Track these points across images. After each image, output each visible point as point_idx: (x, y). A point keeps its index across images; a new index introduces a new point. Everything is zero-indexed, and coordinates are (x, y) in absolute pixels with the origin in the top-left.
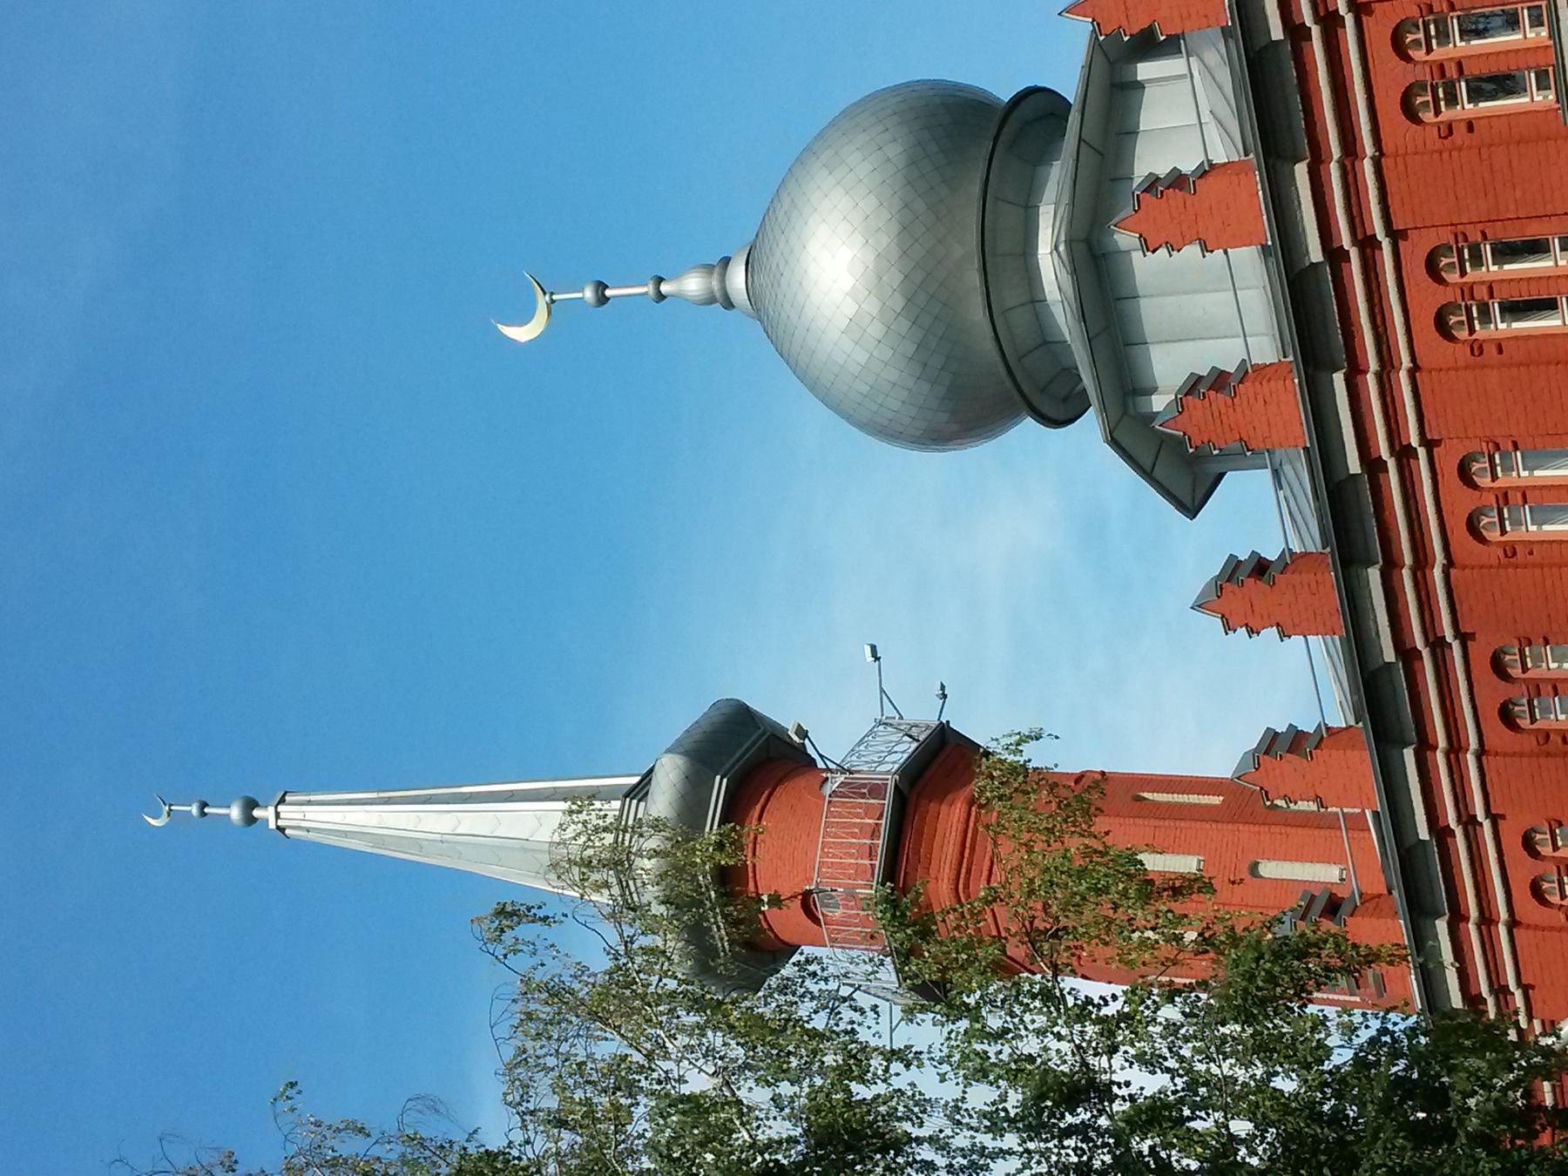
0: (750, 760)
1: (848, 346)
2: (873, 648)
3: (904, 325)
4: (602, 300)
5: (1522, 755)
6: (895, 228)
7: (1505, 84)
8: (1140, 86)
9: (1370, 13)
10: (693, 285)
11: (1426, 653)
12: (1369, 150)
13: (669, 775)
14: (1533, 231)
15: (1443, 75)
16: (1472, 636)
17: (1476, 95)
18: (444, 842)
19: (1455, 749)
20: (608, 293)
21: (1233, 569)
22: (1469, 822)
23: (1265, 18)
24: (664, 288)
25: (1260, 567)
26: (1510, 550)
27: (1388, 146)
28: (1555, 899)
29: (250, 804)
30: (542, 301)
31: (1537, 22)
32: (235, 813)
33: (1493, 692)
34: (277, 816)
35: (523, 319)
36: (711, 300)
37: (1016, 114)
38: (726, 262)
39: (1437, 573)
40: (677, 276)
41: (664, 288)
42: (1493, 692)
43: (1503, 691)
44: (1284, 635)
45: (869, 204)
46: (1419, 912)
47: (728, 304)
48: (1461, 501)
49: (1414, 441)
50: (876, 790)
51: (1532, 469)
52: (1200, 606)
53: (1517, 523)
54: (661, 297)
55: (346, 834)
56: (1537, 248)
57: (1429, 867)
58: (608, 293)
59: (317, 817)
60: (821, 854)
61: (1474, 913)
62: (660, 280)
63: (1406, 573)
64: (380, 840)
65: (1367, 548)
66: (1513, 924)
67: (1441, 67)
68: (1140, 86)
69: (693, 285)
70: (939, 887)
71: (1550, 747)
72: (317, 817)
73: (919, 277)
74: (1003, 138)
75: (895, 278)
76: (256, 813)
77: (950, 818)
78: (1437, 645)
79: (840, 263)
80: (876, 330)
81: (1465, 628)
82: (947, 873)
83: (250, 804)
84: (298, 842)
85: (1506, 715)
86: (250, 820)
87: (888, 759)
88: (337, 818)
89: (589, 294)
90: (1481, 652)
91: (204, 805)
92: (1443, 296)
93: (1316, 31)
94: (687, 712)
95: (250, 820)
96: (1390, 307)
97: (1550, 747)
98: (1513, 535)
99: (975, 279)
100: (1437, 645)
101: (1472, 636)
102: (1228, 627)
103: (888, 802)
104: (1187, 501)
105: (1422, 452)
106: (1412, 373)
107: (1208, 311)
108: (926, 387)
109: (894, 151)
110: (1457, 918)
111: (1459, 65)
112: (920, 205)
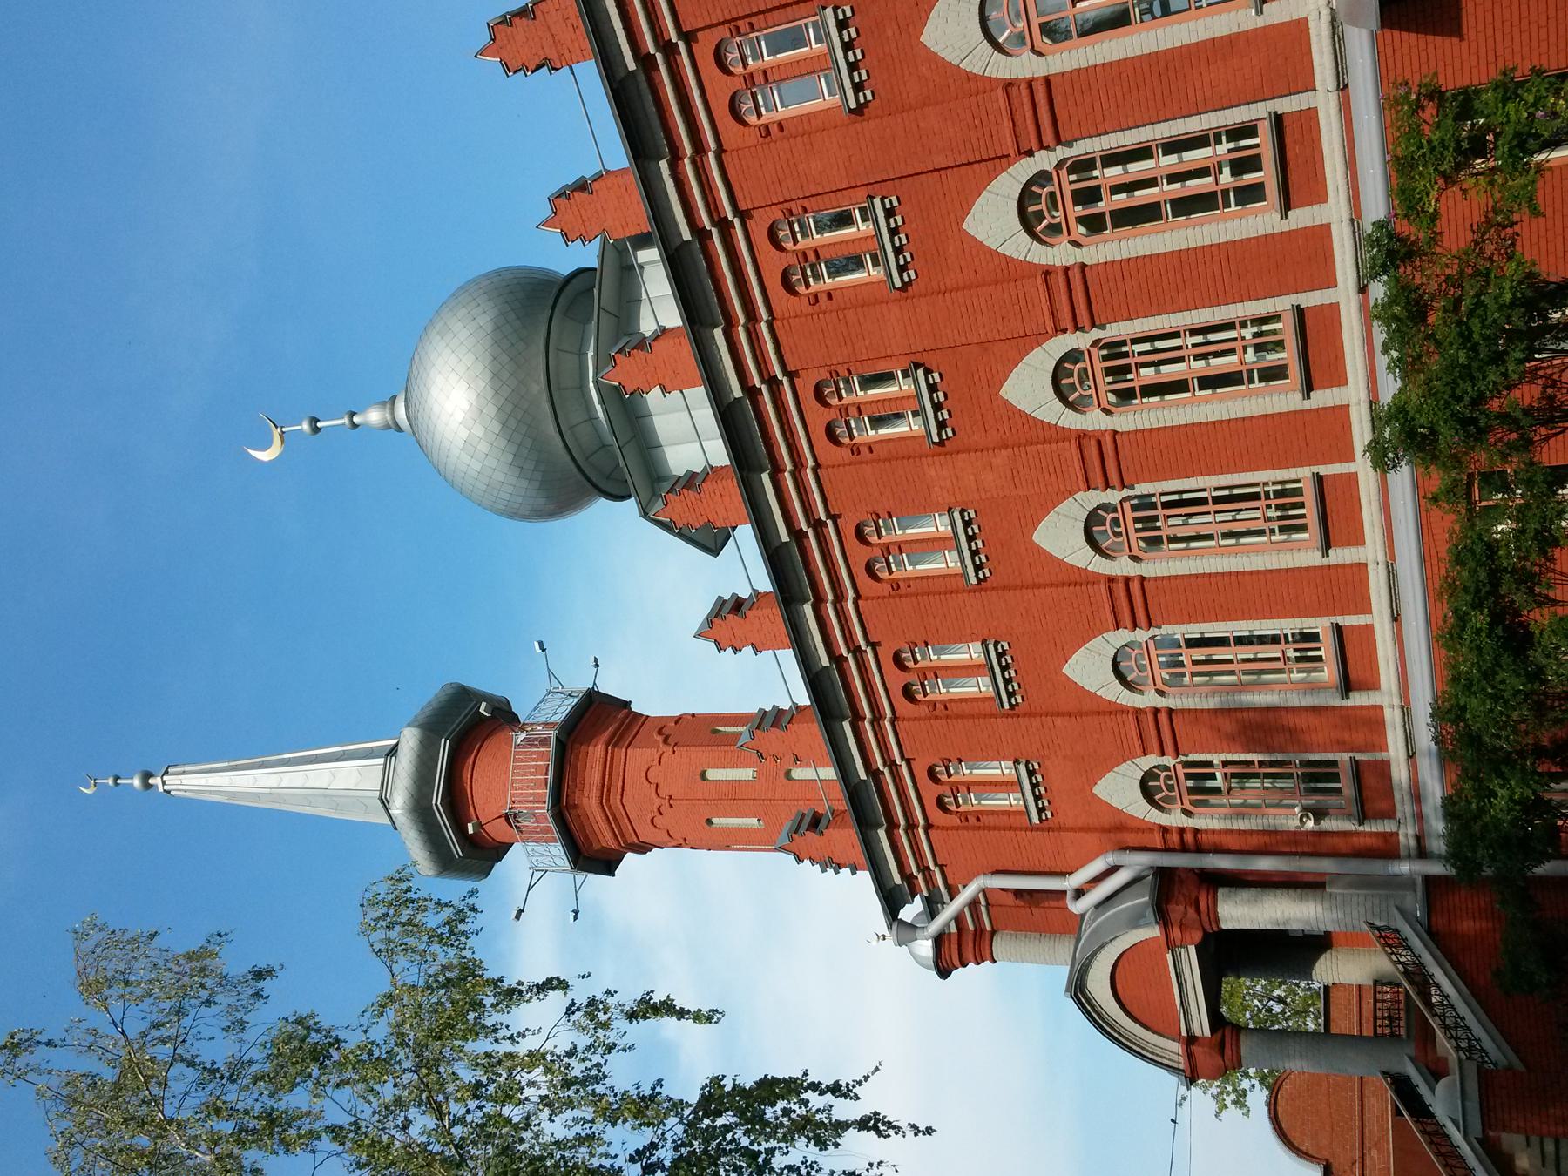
0: (466, 726)
1: (466, 459)
2: (541, 644)
3: (502, 443)
4: (316, 430)
5: (919, 719)
6: (488, 375)
7: (857, 263)
8: (641, 267)
9: (751, 217)
10: (374, 416)
11: (850, 657)
12: (765, 316)
13: (409, 740)
14: (882, 367)
15: (806, 260)
16: (879, 644)
17: (835, 271)
18: (272, 794)
19: (877, 718)
20: (319, 425)
21: (721, 604)
22: (892, 765)
23: (676, 225)
24: (356, 419)
25: (738, 605)
26: (895, 585)
27: (777, 311)
28: (953, 808)
29: (147, 775)
30: (276, 432)
31: (864, 220)
32: (137, 782)
33: (897, 679)
34: (164, 783)
35: (265, 446)
36: (387, 427)
37: (569, 287)
38: (394, 399)
39: (850, 604)
40: (364, 410)
41: (356, 419)
42: (897, 679)
43: (905, 678)
44: (757, 651)
45: (469, 359)
46: (865, 825)
47: (400, 430)
48: (860, 554)
49: (823, 517)
50: (545, 742)
51: (904, 528)
52: (699, 635)
53: (899, 564)
54: (355, 426)
55: (210, 792)
56: (886, 378)
57: (870, 798)
58: (319, 425)
59: (188, 782)
60: (513, 781)
61: (902, 822)
62: (353, 414)
63: (829, 605)
64: (233, 795)
65: (802, 591)
66: (928, 826)
67: (804, 254)
68: (641, 267)
69: (374, 416)
70: (589, 802)
71: (937, 712)
72: (188, 782)
73: (509, 408)
74: (559, 305)
75: (491, 410)
76: (151, 781)
77: (595, 753)
78: (857, 652)
79: (457, 399)
80: (483, 447)
81: (873, 639)
82: (595, 793)
83: (147, 775)
84: (179, 798)
85: (907, 692)
86: (147, 786)
87: (559, 710)
88: (203, 782)
89: (305, 426)
90: (886, 654)
91: (117, 778)
92: (830, 415)
93: (715, 232)
94: (426, 693)
95: (147, 786)
96: (796, 425)
97: (937, 712)
98: (897, 574)
99: (546, 407)
100: (857, 652)
101: (879, 644)
102: (720, 648)
103: (551, 750)
104: (711, 545)
105: (829, 522)
106: (815, 470)
107: (687, 434)
108: (525, 483)
109: (485, 320)
110: (892, 826)
111: (816, 252)
112: (505, 358)
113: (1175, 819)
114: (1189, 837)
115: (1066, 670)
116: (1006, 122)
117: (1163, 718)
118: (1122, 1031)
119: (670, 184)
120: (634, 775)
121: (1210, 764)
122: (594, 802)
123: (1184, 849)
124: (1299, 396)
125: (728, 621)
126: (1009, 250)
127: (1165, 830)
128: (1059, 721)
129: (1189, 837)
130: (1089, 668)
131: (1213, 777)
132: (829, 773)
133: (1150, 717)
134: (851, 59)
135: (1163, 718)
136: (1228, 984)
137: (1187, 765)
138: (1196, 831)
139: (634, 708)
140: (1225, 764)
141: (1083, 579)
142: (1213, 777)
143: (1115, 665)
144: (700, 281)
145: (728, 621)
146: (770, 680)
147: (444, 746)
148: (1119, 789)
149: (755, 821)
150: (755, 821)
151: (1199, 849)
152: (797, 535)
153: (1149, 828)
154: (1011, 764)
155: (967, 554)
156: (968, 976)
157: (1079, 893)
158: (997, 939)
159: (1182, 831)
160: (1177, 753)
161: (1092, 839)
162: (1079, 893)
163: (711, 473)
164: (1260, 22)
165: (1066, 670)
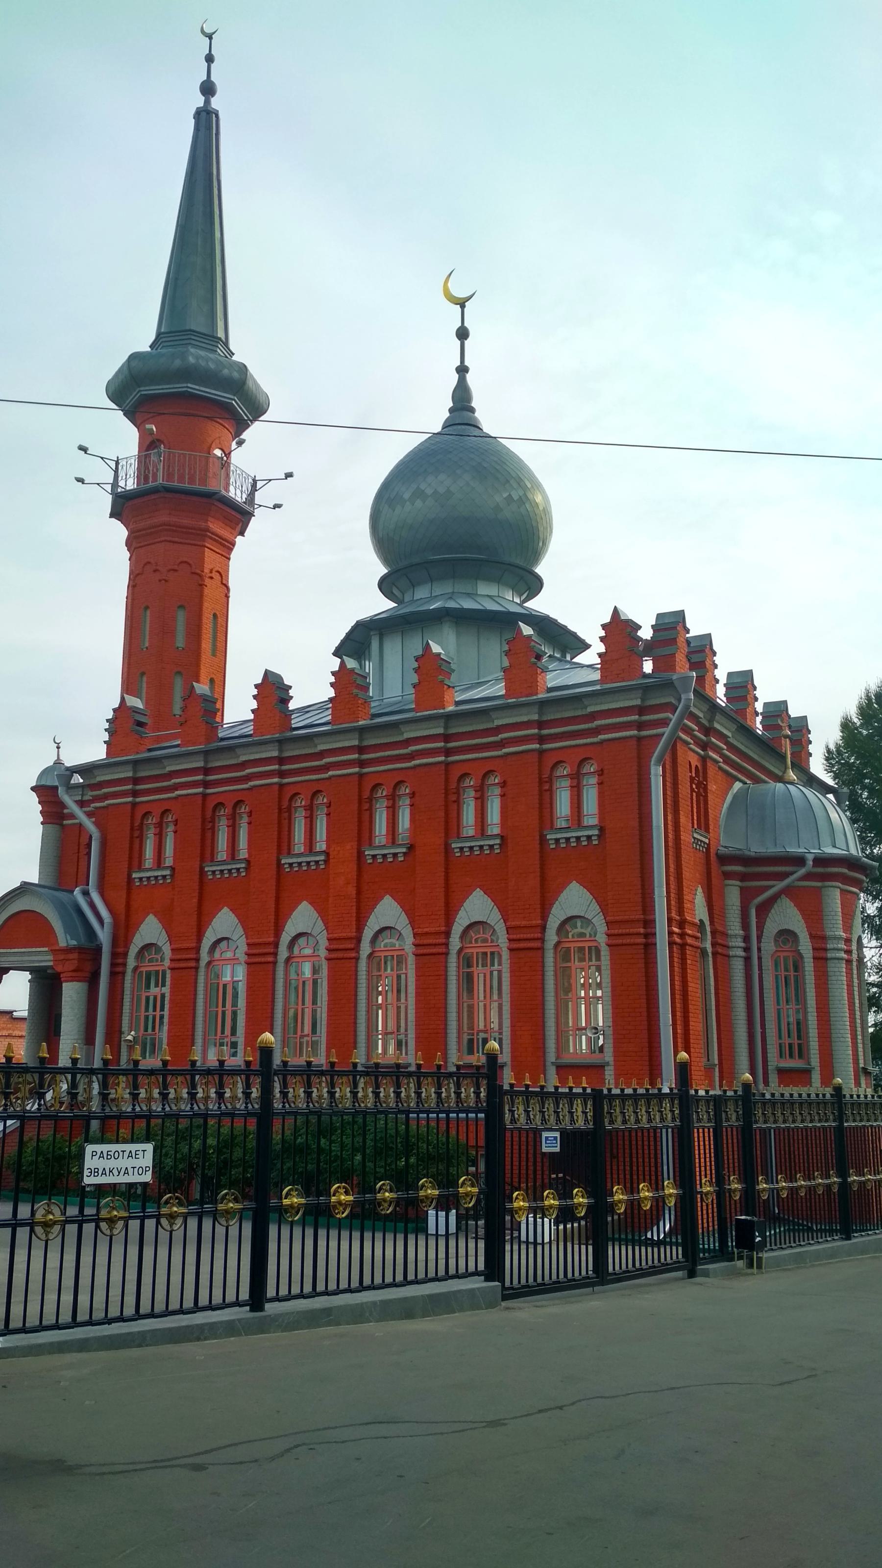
18: (60, 922)
113: (131, 962)
114: (119, 969)
115: (226, 910)
116: (524, 923)
117: (192, 964)
119: (525, 719)
121: (164, 985)
123: (113, 965)
125: (273, 691)
126: (461, 913)
127: (126, 954)
128: (195, 900)
129: (119, 969)
131: (157, 985)
133: (193, 956)
134: (572, 840)
135: (192, 964)
136: (27, 975)
137: (164, 972)
140: (163, 996)
142: (157, 985)
143: (227, 939)
145: (273, 691)
146: (238, 706)
148: (150, 930)
149: (147, 644)
150: (147, 644)
153: (127, 946)
154: (171, 864)
156: (33, 806)
157: (86, 893)
158: (57, 827)
161: (121, 908)
162: (86, 893)
164: (548, 1064)
165: (226, 910)
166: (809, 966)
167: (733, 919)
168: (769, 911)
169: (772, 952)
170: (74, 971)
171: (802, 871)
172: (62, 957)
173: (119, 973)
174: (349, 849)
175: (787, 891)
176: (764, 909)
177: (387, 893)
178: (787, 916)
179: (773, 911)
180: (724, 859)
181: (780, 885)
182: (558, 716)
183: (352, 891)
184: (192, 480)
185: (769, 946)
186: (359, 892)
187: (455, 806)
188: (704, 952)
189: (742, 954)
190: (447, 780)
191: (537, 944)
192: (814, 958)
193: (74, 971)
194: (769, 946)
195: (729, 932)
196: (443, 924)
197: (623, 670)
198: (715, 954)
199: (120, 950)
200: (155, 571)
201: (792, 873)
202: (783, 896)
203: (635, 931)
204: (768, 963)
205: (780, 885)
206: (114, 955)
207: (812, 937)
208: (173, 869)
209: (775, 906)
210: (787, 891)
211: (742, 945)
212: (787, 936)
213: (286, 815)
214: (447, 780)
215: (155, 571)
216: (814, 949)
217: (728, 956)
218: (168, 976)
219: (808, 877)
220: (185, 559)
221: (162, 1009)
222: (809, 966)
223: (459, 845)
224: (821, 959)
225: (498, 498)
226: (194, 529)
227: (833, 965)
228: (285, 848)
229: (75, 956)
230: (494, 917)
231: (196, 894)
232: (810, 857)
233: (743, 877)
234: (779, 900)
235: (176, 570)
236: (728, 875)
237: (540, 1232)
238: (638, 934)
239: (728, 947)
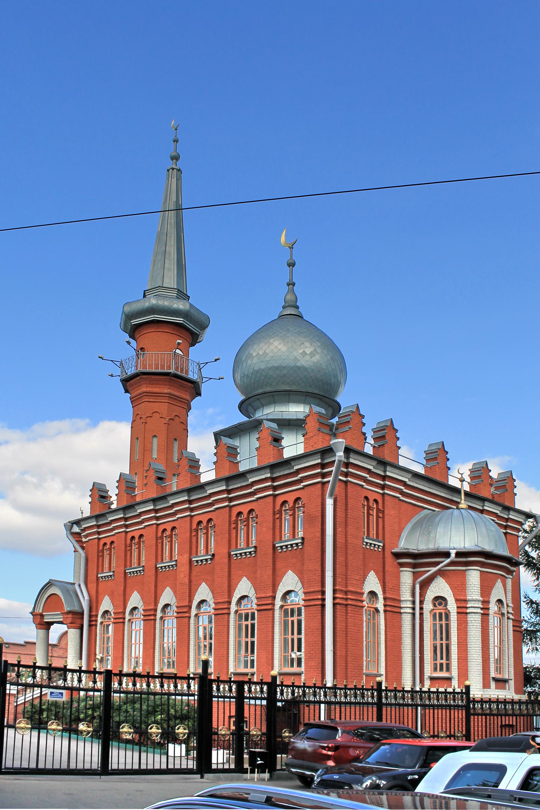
82: (149, 389)
113: (100, 620)
114: (93, 623)
118: (43, 595)
119: (263, 477)
120: (156, 407)
122: (144, 389)
123: (90, 621)
124: (429, 675)
128: (122, 588)
129: (93, 623)
130: (290, 581)
132: (175, 489)
133: (121, 616)
138: (96, 625)
139: (196, 402)
141: (156, 603)
144: (240, 483)
147: (179, 320)
151: (90, 626)
152: (298, 471)
153: (97, 611)
155: (136, 570)
159: (96, 621)
160: (258, 611)
163: (281, 451)
166: (454, 617)
167: (405, 591)
168: (429, 586)
169: (429, 610)
170: (70, 623)
171: (448, 561)
172: (66, 616)
173: (93, 625)
174: (186, 557)
175: (440, 573)
176: (425, 585)
177: (203, 581)
178: (440, 587)
179: (431, 585)
180: (398, 555)
181: (434, 570)
182: (281, 474)
183: (187, 580)
184: (163, 367)
185: (428, 606)
186: (190, 581)
187: (234, 531)
188: (377, 610)
189: (410, 611)
190: (230, 516)
191: (269, 607)
192: (458, 613)
193: (70, 623)
194: (428, 606)
195: (402, 599)
196: (227, 597)
197: (315, 443)
198: (385, 611)
199: (94, 613)
200: (141, 418)
201: (442, 562)
202: (438, 576)
203: (315, 597)
204: (427, 616)
205: (434, 570)
206: (90, 616)
207: (457, 600)
208: (255, 547)
209: (433, 582)
210: (440, 573)
211: (411, 606)
212: (440, 600)
213: (160, 541)
214: (230, 516)
215: (141, 418)
216: (458, 607)
217: (401, 613)
218: (303, 611)
219: (452, 563)
220: (156, 410)
221: (299, 633)
222: (454, 617)
223: (235, 553)
224: (462, 613)
225: (295, 353)
226: (161, 393)
227: (471, 617)
228: (159, 558)
229: (70, 616)
230: (252, 593)
231: (123, 585)
232: (453, 553)
233: (414, 566)
234: (435, 579)
235: (173, 419)
236: (402, 565)
237: (452, 739)
238: (318, 599)
239: (401, 608)
